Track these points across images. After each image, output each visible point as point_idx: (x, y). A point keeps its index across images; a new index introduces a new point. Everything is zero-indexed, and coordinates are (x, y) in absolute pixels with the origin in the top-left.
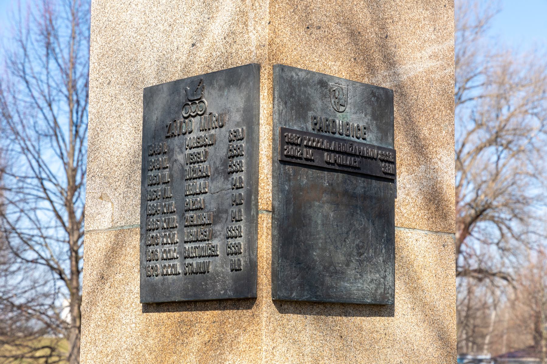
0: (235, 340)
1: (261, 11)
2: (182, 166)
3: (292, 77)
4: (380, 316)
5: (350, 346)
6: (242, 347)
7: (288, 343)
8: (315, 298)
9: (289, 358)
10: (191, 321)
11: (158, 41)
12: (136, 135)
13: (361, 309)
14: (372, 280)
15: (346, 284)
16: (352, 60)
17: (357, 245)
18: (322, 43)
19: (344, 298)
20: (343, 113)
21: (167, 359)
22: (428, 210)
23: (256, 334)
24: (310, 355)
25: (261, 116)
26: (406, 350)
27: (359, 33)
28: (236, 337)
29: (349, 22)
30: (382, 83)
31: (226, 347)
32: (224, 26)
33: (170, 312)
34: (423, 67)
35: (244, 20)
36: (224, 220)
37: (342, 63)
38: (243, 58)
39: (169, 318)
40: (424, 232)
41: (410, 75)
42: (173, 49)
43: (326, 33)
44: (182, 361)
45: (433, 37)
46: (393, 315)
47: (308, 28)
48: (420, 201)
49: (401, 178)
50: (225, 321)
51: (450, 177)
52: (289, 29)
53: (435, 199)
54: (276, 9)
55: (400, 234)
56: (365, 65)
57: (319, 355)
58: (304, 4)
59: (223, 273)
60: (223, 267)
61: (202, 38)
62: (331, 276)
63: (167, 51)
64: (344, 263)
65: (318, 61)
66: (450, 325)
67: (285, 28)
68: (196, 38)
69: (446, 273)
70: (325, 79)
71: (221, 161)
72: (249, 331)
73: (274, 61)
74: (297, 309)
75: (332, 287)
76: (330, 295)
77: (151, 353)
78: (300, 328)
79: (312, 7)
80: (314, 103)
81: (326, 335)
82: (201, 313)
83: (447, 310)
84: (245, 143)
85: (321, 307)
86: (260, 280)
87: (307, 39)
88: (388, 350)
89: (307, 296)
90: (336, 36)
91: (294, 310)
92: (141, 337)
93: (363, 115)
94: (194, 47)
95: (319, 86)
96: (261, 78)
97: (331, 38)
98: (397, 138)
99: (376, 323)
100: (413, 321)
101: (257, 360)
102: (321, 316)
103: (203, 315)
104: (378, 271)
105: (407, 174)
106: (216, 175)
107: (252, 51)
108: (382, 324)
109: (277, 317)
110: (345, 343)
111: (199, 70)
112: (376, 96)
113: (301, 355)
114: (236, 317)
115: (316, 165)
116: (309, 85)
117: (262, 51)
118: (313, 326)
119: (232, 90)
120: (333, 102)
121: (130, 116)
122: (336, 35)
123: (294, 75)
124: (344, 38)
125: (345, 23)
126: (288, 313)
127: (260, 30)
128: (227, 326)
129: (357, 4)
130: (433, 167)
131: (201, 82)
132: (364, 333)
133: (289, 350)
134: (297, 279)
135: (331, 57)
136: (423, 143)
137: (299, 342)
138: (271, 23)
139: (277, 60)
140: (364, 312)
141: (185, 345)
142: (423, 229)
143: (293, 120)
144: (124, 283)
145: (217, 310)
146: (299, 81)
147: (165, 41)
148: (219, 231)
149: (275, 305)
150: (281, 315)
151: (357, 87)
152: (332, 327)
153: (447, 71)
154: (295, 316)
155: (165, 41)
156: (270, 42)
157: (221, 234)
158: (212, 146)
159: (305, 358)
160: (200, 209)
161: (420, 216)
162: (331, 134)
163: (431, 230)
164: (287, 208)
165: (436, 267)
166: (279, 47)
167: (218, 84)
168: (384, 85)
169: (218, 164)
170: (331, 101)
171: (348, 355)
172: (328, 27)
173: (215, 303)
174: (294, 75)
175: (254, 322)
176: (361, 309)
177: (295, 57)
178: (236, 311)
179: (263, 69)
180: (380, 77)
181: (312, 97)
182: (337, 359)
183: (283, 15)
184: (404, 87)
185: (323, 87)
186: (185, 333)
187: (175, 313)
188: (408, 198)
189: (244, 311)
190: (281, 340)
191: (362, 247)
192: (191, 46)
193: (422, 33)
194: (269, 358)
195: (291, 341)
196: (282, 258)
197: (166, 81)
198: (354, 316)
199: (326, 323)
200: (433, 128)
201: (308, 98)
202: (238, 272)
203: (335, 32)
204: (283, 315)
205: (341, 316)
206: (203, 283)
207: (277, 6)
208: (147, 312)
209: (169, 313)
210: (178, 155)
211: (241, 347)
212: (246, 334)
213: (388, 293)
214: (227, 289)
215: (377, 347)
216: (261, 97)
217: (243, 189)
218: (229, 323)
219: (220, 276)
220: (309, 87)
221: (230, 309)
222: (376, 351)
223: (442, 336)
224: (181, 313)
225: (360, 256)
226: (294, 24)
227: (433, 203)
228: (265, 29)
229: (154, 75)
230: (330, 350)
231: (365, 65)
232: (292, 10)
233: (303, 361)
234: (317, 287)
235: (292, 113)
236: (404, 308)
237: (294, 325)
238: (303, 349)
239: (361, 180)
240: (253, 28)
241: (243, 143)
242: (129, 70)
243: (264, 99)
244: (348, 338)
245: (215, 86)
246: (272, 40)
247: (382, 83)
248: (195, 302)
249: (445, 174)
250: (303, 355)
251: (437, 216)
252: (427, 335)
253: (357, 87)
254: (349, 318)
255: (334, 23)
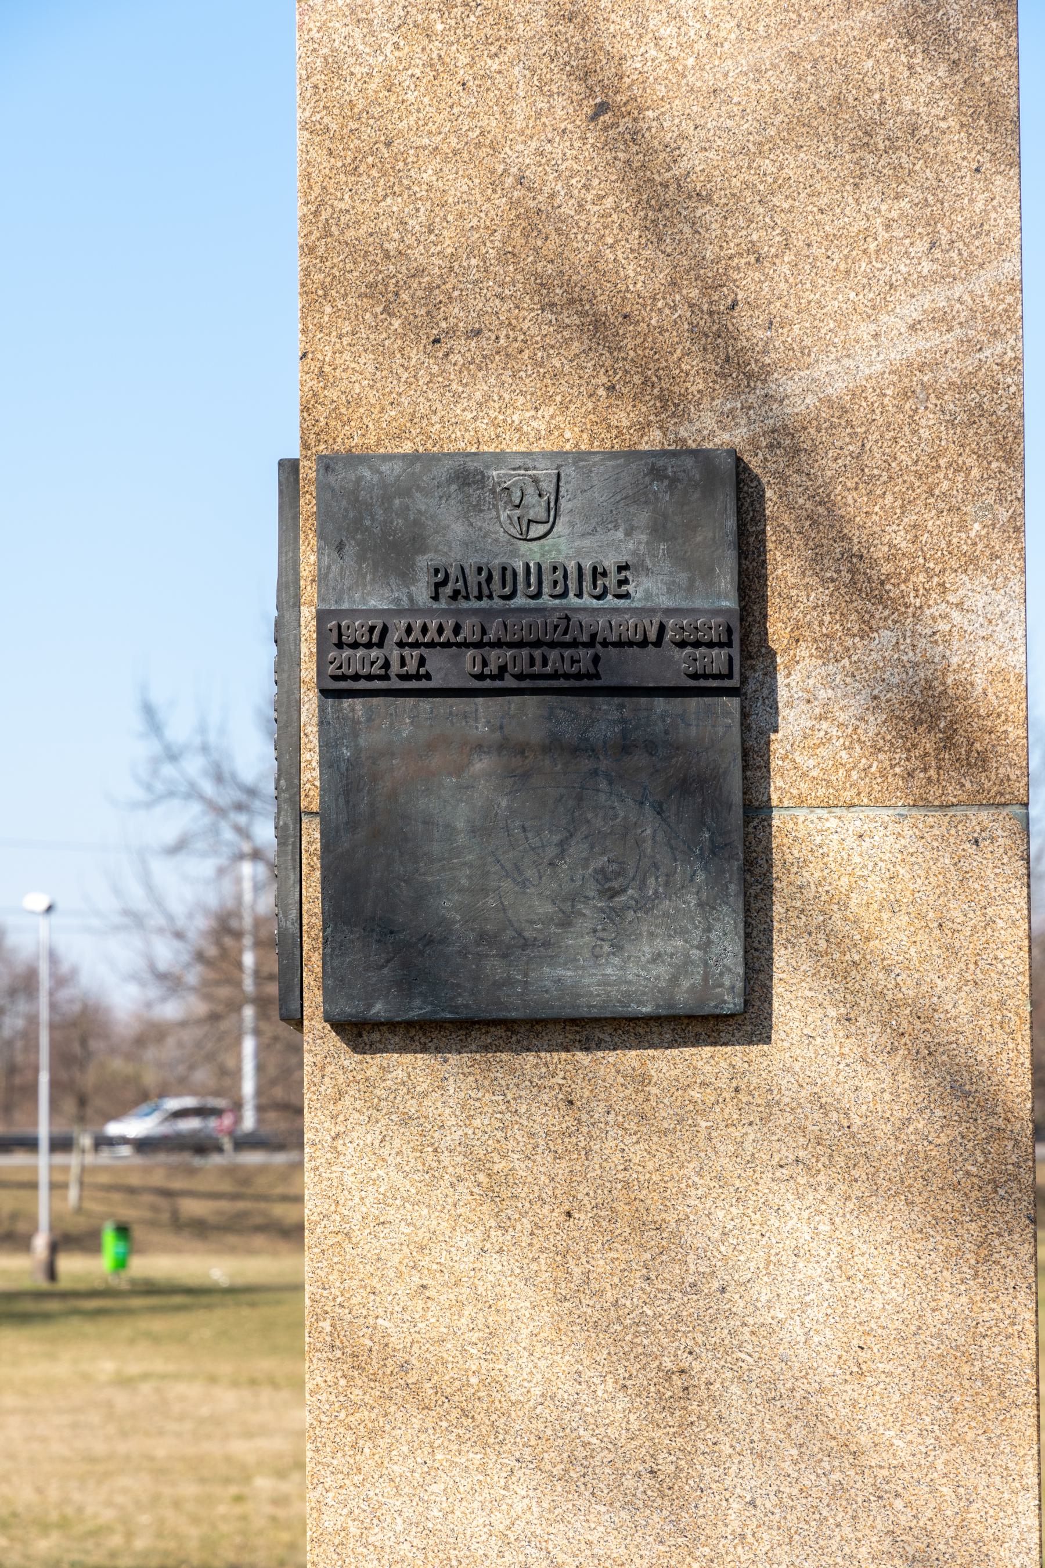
3: (360, 479)
4: (714, 1044)
5: (602, 1125)
7: (383, 1122)
8: (450, 1012)
9: (390, 1159)
13: (641, 1031)
14: (657, 958)
15: (561, 972)
16: (601, 392)
17: (602, 871)
18: (487, 369)
19: (552, 1007)
20: (542, 541)
22: (909, 750)
24: (459, 1149)
26: (816, 1128)
27: (625, 317)
29: (585, 297)
30: (718, 432)
34: (883, 362)
37: (564, 407)
40: (891, 812)
41: (830, 390)
43: (502, 341)
45: (926, 267)
46: (767, 1040)
47: (437, 341)
48: (872, 731)
49: (796, 676)
51: (1001, 647)
52: (372, 356)
53: (935, 717)
54: (326, 318)
55: (791, 825)
56: (648, 398)
57: (489, 1149)
58: (420, 283)
62: (504, 956)
64: (552, 919)
65: (475, 419)
66: (1004, 1056)
67: (356, 358)
69: (984, 915)
70: (472, 465)
73: (322, 447)
74: (412, 1039)
75: (509, 982)
76: (502, 1003)
78: (425, 1085)
79: (449, 286)
80: (437, 533)
81: (514, 1099)
83: (989, 1016)
85: (500, 1032)
87: (435, 369)
88: (749, 1129)
89: (421, 1008)
90: (537, 343)
91: (402, 1044)
93: (620, 534)
95: (454, 487)
97: (522, 351)
98: (779, 572)
99: (700, 1063)
100: (846, 1050)
102: (498, 1054)
104: (683, 932)
105: (820, 662)
108: (723, 1064)
109: (346, 1063)
110: (584, 1117)
112: (666, 477)
113: (430, 1149)
115: (438, 686)
116: (419, 489)
118: (471, 1078)
120: (503, 516)
122: (539, 338)
123: (367, 474)
124: (567, 342)
125: (571, 302)
126: (381, 1051)
129: (616, 242)
130: (929, 631)
132: (654, 1090)
133: (387, 1138)
134: (385, 971)
135: (521, 400)
136: (886, 568)
137: (422, 1120)
138: (310, 356)
139: (331, 441)
140: (655, 1036)
142: (888, 803)
143: (365, 586)
146: (384, 486)
149: (338, 1034)
150: (358, 1057)
151: (594, 465)
152: (536, 1080)
153: (987, 353)
154: (408, 1058)
156: (308, 401)
159: (442, 1158)
161: (873, 770)
162: (496, 600)
163: (921, 804)
164: (347, 802)
165: (941, 901)
166: (337, 408)
168: (726, 436)
170: (498, 517)
171: (596, 1148)
172: (510, 324)
174: (367, 474)
176: (641, 1031)
177: (394, 424)
180: (709, 421)
181: (433, 518)
182: (555, 1158)
183: (349, 328)
184: (805, 429)
185: (469, 485)
188: (825, 725)
190: (362, 1118)
191: (618, 874)
193: (879, 266)
194: (323, 1160)
195: (393, 1117)
196: (336, 925)
198: (615, 1049)
199: (516, 1070)
200: (930, 523)
201: (416, 523)
203: (534, 331)
204: (368, 1057)
205: (568, 1051)
207: (328, 309)
213: (721, 985)
215: (704, 1124)
220: (418, 495)
222: (702, 1136)
223: (967, 1087)
225: (612, 897)
226: (387, 343)
227: (930, 729)
230: (531, 1135)
231: (648, 398)
232: (379, 309)
233: (434, 1165)
234: (458, 985)
235: (360, 568)
236: (810, 1019)
237: (405, 1079)
238: (437, 1135)
239: (609, 704)
244: (594, 1104)
246: (314, 395)
247: (718, 432)
249: (981, 643)
250: (436, 1150)
251: (947, 764)
252: (906, 1085)
253: (594, 465)
254: (600, 1054)
255: (532, 310)
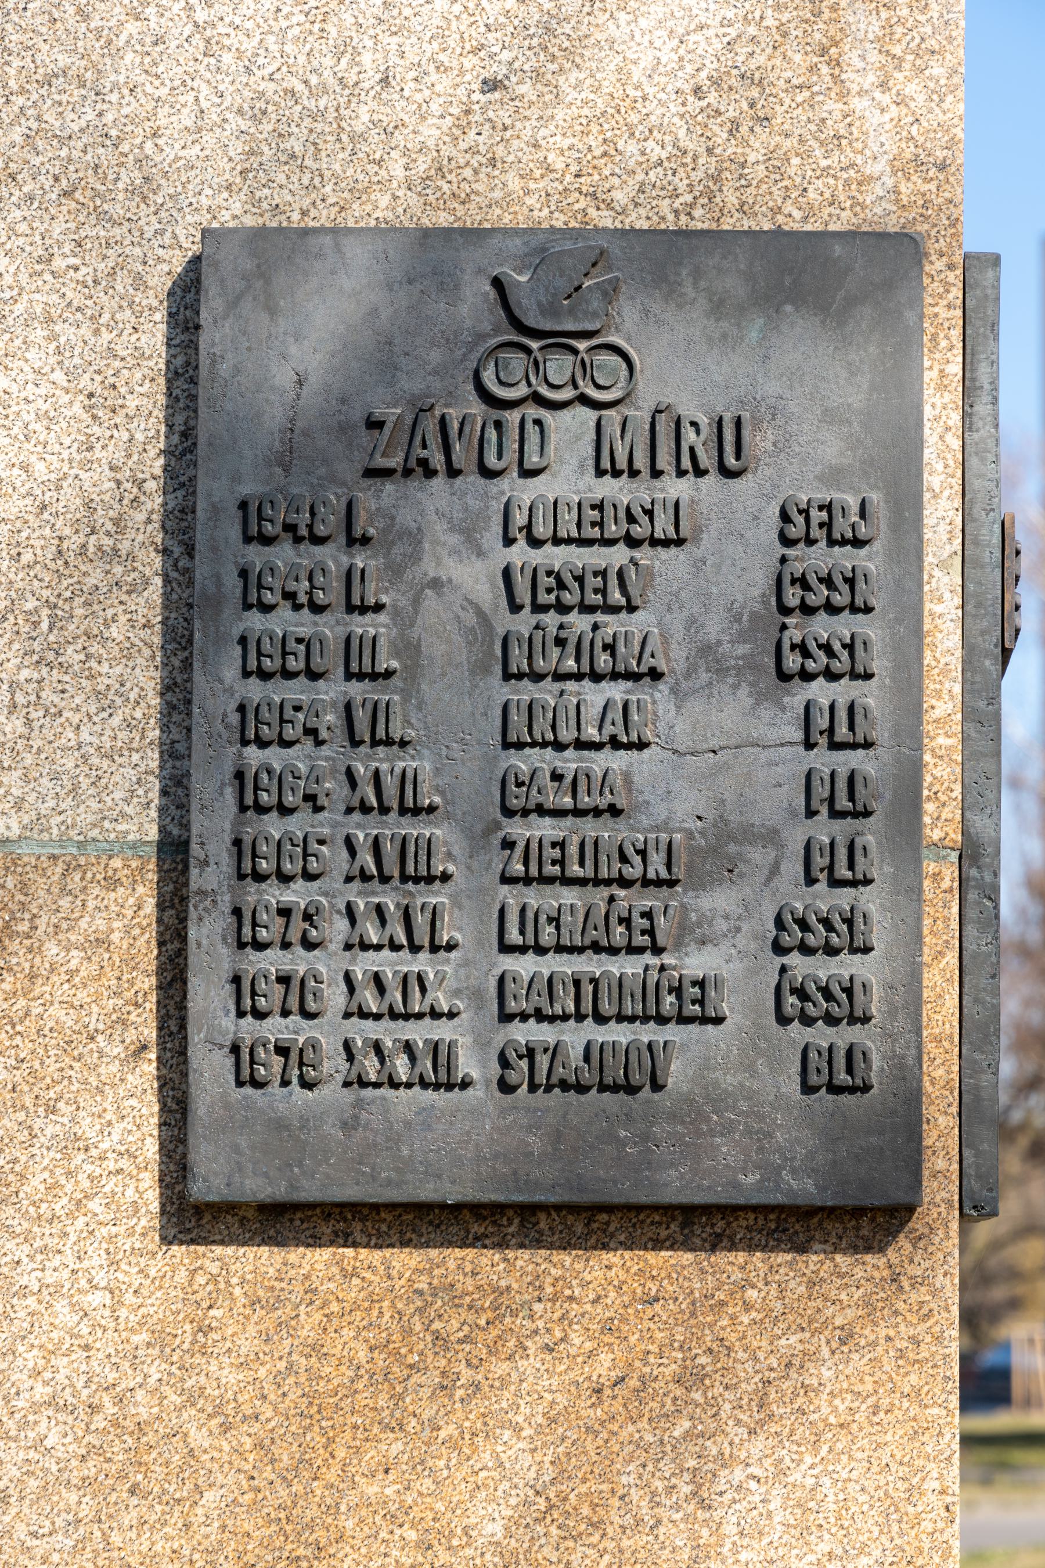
0: (787, 1377)
1: (922, 18)
2: (480, 613)
6: (823, 1408)
10: (500, 1292)
11: (250, 25)
12: (96, 430)
21: (341, 1453)
23: (911, 1356)
25: (928, 454)
28: (789, 1365)
31: (727, 1406)
32: (693, 38)
33: (355, 1245)
35: (817, 36)
36: (761, 876)
38: (812, 194)
39: (346, 1275)
42: (352, 78)
44: (441, 1463)
50: (721, 1295)
59: (750, 1095)
60: (751, 1069)
61: (554, 67)
63: (314, 80)
68: (506, 56)
71: (737, 618)
72: (874, 1344)
77: (226, 1428)
82: (567, 1258)
84: (879, 559)
86: (935, 1134)
92: (156, 1352)
94: (497, 95)
96: (929, 300)
101: (919, 1463)
103: (578, 1266)
106: (704, 677)
107: (870, 179)
111: (530, 201)
114: (792, 1284)
117: (932, 186)
119: (793, 325)
121: (54, 337)
127: (921, 98)
128: (733, 1317)
131: (598, 260)
141: (460, 1393)
144: (28, 1101)
145: (671, 1248)
147: (296, 31)
148: (727, 917)
155: (296, 31)
157: (738, 929)
158: (673, 550)
160: (614, 811)
167: (703, 284)
169: (714, 629)
173: (657, 1218)
175: (901, 1306)
178: (789, 1257)
179: (940, 264)
186: (460, 1341)
187: (388, 1252)
189: (839, 1258)
192: (476, 86)
197: (304, 213)
202: (845, 1099)
206: (623, 1134)
208: (192, 1242)
209: (349, 1252)
210: (450, 562)
211: (825, 1410)
212: (855, 1356)
214: (781, 1168)
216: (930, 376)
217: (871, 752)
218: (748, 1307)
219: (734, 1109)
221: (751, 1248)
224: (434, 1253)
228: (950, 98)
229: (224, 170)
240: (871, 78)
241: (869, 558)
242: (39, 118)
243: (942, 387)
245: (691, 293)
248: (528, 1211)
